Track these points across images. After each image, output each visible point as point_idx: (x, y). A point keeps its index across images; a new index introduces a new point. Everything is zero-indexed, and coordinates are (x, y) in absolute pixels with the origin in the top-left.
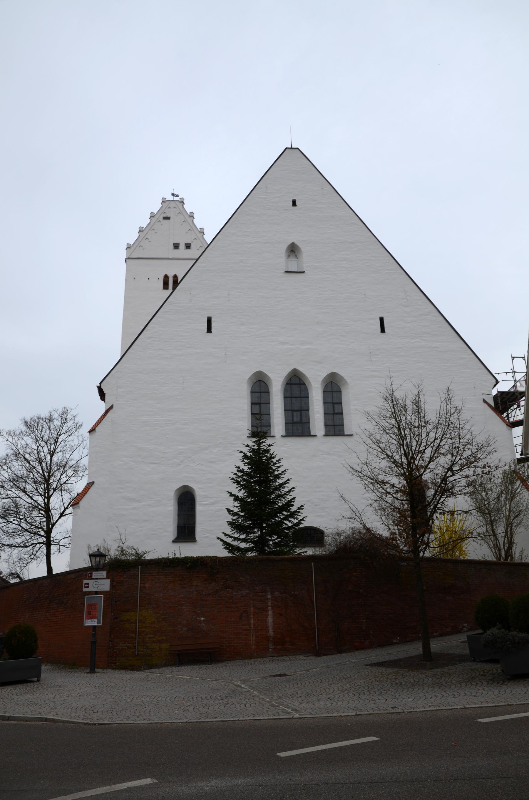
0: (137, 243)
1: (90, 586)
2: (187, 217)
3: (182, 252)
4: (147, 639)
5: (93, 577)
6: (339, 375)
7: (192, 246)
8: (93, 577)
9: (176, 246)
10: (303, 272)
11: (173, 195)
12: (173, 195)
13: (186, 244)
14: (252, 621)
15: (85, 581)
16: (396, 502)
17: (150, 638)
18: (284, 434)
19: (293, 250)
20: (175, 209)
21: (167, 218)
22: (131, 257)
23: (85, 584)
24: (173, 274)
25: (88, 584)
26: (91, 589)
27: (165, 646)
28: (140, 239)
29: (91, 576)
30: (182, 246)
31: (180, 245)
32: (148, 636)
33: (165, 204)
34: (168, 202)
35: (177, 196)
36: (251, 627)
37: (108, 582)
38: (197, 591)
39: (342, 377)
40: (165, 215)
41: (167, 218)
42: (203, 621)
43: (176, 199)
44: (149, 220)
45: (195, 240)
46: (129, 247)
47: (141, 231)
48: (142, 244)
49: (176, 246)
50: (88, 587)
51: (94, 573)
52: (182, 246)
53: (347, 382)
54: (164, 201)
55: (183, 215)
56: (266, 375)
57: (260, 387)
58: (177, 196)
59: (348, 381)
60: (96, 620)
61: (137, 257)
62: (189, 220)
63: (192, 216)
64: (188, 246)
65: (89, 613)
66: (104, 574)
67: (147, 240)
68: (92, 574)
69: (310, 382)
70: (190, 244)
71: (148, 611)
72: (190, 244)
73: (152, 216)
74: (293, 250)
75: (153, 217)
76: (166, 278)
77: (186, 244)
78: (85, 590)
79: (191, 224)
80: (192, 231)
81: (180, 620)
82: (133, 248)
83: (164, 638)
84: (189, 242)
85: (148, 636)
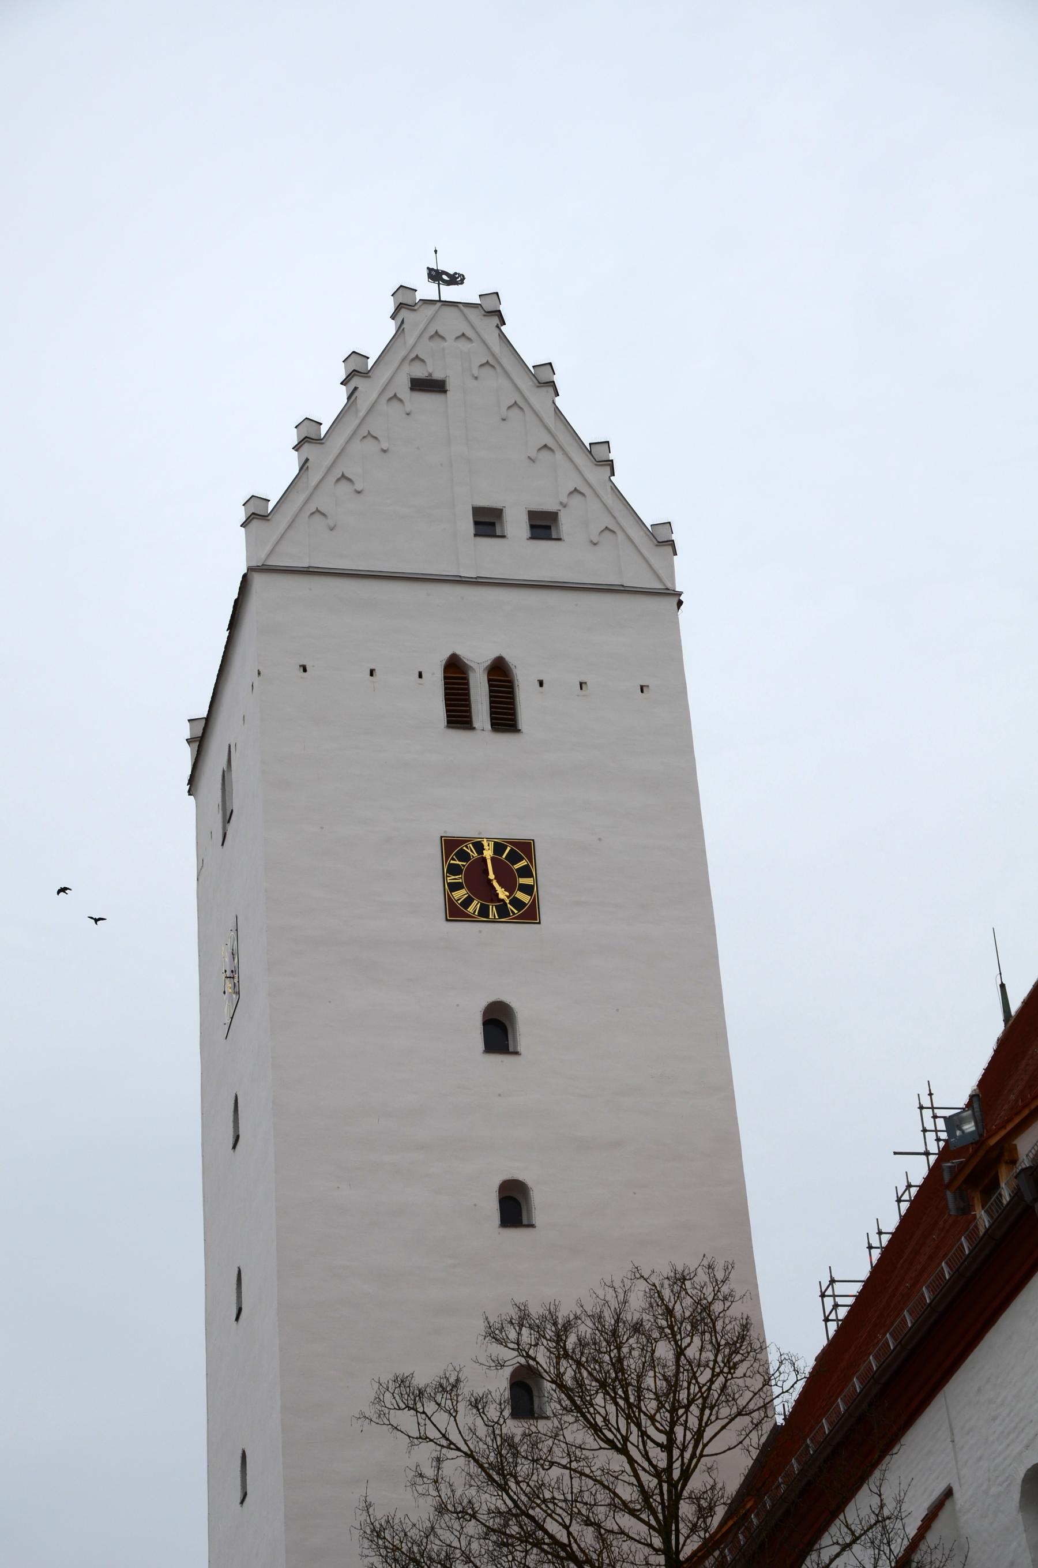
0: (298, 499)
2: (525, 384)
3: (515, 553)
7: (566, 524)
9: (487, 522)
11: (435, 275)
12: (435, 275)
13: (532, 515)
18: (529, 535)
20: (464, 346)
21: (429, 386)
22: (273, 562)
30: (516, 525)
33: (415, 320)
34: (431, 310)
35: (456, 279)
43: (450, 293)
44: (343, 392)
45: (577, 499)
46: (257, 514)
47: (309, 437)
48: (321, 502)
49: (487, 522)
52: (516, 525)
54: (405, 303)
58: (456, 279)
61: (304, 563)
62: (538, 398)
63: (544, 379)
64: (543, 526)
67: (344, 486)
70: (553, 516)
72: (553, 516)
75: (365, 374)
76: (455, 671)
77: (532, 515)
79: (550, 420)
80: (559, 456)
82: (281, 522)
84: (550, 506)
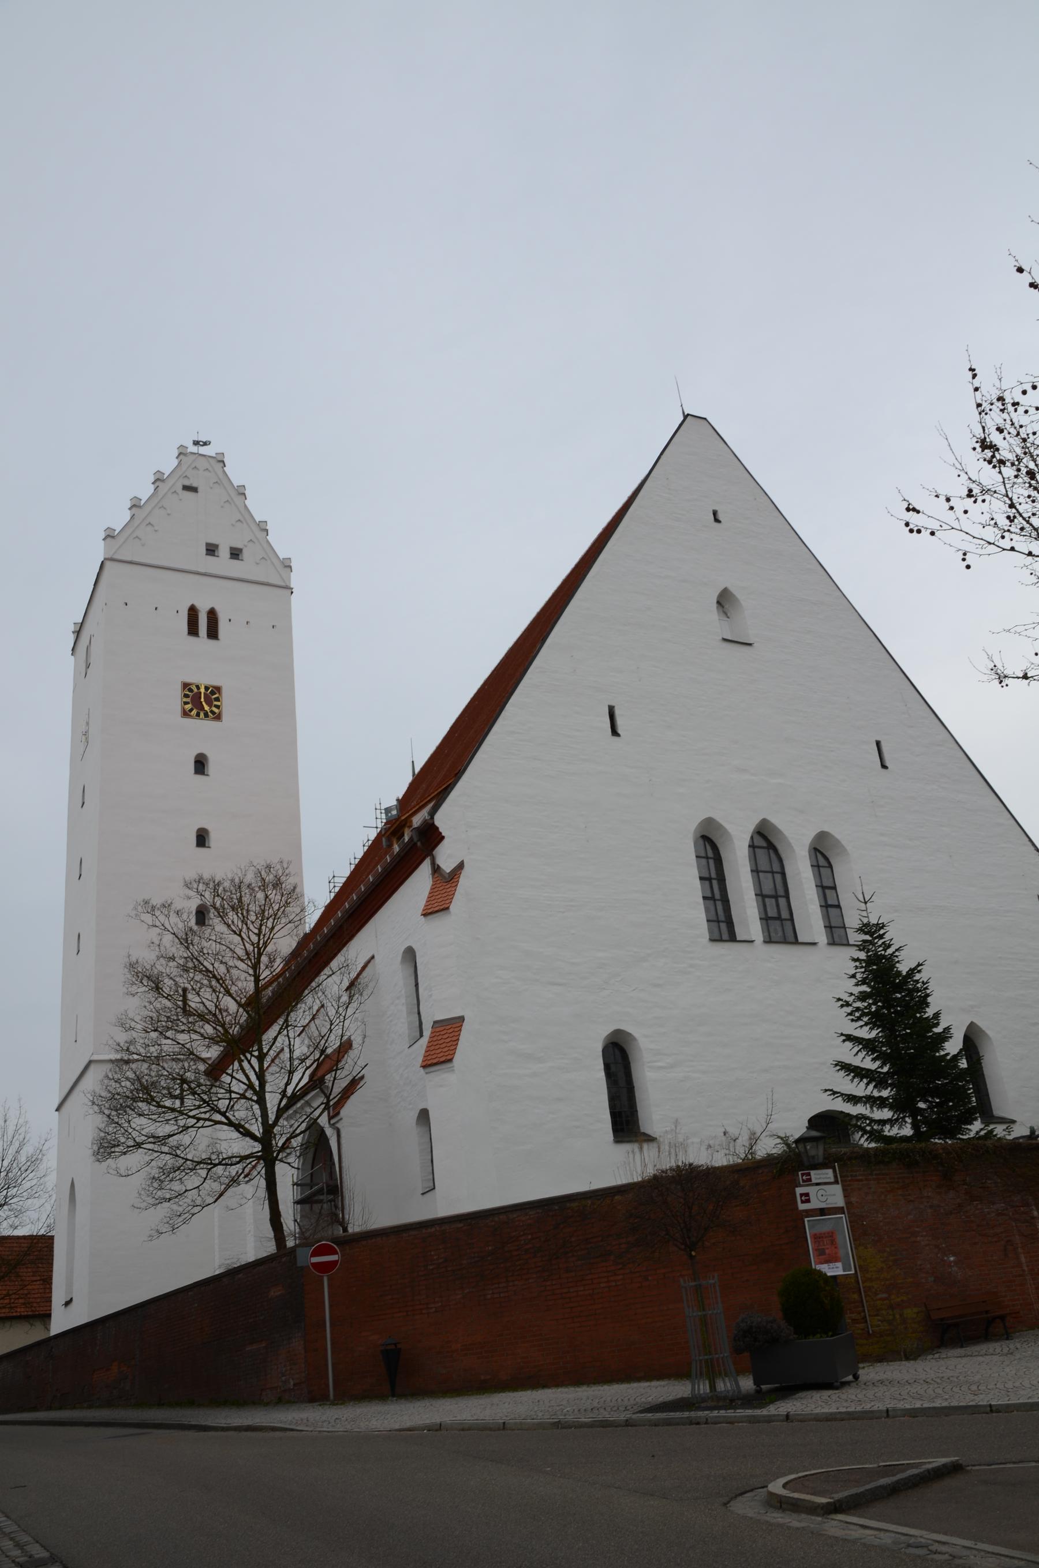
1: (812, 1197)
2: (233, 494)
3: (223, 563)
4: (878, 1302)
5: (814, 1181)
6: (833, 836)
7: (245, 554)
8: (814, 1181)
9: (211, 550)
10: (750, 644)
13: (208, 544)
14: (1023, 1259)
15: (799, 1191)
16: (234, 1145)
17: (881, 1299)
19: (725, 601)
21: (192, 489)
22: (116, 557)
23: (802, 1195)
24: (208, 608)
25: (807, 1195)
26: (815, 1204)
27: (910, 1313)
28: (136, 522)
29: (810, 1180)
30: (224, 552)
31: (220, 547)
32: (880, 1296)
34: (194, 457)
36: (1024, 1271)
37: (837, 1190)
38: (931, 1207)
39: (838, 841)
40: (187, 483)
41: (192, 489)
42: (954, 1261)
49: (211, 550)
50: (808, 1201)
51: (813, 1173)
52: (224, 552)
53: (845, 850)
54: (182, 453)
55: (225, 488)
56: (719, 827)
57: (709, 845)
59: (849, 848)
60: (839, 1265)
62: (238, 500)
63: (241, 492)
65: (820, 1252)
66: (828, 1174)
68: (809, 1174)
69: (789, 845)
70: (241, 550)
71: (866, 1248)
72: (241, 550)
73: (159, 479)
74: (725, 601)
76: (193, 613)
77: (208, 544)
78: (802, 1207)
81: (919, 1263)
83: (905, 1298)
84: (239, 546)
85: (880, 1296)
